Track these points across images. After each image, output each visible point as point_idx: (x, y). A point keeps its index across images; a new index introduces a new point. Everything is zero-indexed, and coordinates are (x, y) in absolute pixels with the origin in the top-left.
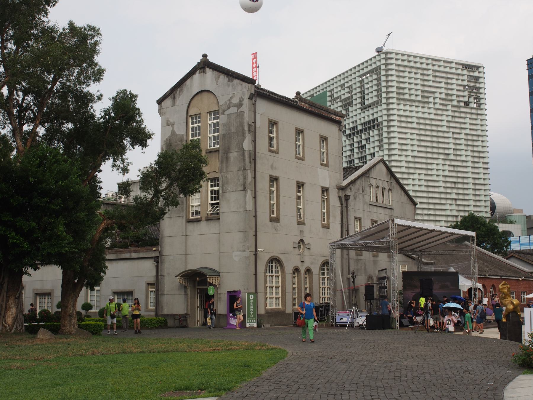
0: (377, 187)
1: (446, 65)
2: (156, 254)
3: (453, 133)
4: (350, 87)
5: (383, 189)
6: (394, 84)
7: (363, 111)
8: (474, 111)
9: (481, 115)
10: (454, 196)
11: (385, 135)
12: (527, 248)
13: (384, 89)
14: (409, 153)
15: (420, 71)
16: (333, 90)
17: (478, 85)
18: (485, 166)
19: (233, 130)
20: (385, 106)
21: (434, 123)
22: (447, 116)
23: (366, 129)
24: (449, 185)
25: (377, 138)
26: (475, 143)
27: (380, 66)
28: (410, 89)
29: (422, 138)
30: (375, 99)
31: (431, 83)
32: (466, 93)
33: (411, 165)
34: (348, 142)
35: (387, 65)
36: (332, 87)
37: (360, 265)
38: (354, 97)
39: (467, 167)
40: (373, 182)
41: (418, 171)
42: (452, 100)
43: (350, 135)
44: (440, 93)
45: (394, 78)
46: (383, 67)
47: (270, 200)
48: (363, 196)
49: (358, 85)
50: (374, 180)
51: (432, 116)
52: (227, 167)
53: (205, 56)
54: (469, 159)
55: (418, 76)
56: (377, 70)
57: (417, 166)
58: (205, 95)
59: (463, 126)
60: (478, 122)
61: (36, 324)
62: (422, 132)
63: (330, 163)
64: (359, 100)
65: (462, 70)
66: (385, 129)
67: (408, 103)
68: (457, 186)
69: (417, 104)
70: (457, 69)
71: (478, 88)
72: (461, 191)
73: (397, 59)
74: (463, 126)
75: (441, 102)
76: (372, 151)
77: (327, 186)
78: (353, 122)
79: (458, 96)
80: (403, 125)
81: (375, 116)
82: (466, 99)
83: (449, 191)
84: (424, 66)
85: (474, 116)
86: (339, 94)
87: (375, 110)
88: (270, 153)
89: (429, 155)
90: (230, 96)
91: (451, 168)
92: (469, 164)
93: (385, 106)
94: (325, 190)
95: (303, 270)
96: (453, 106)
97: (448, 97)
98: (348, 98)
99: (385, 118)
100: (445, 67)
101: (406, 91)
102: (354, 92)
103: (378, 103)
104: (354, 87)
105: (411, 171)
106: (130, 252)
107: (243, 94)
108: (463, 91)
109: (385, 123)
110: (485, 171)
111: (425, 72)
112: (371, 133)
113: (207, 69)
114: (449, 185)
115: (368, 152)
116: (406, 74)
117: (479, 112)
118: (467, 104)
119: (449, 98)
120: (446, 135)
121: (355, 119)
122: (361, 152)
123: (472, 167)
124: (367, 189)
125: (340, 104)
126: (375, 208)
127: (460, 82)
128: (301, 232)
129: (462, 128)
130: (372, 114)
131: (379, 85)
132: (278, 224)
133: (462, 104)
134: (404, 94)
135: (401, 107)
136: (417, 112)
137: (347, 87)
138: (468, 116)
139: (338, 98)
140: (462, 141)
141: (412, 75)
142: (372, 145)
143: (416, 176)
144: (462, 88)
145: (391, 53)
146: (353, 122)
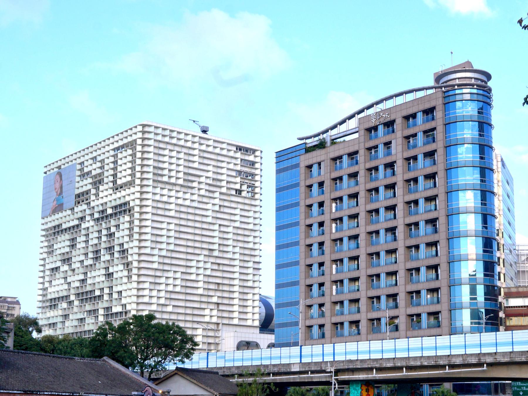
1: (216, 145)
3: (220, 225)
4: (102, 161)
6: (151, 162)
7: (115, 191)
8: (247, 201)
11: (137, 222)
13: (138, 168)
14: (164, 246)
16: (83, 162)
17: (253, 171)
18: (256, 266)
20: (138, 188)
22: (214, 205)
25: (127, 225)
27: (135, 140)
28: (170, 170)
29: (183, 229)
30: (129, 178)
31: (196, 165)
32: (238, 180)
33: (167, 261)
35: (143, 139)
38: (106, 174)
42: (221, 187)
43: (98, 219)
45: (151, 156)
46: (139, 142)
49: (112, 159)
51: (195, 204)
54: (237, 256)
56: (132, 145)
57: (174, 262)
61: (136, 393)
62: (183, 222)
64: (111, 178)
66: (137, 216)
68: (221, 288)
69: (178, 188)
70: (229, 150)
71: (253, 175)
75: (207, 188)
76: (121, 241)
79: (228, 182)
80: (160, 212)
82: (238, 187)
87: (128, 191)
89: (190, 250)
91: (215, 267)
93: (138, 188)
96: (221, 193)
97: (216, 183)
98: (100, 175)
99: (138, 202)
100: (215, 147)
101: (166, 172)
103: (131, 184)
104: (107, 161)
105: (166, 268)
108: (235, 177)
109: (137, 209)
110: (256, 272)
112: (122, 220)
117: (253, 202)
118: (239, 192)
120: (211, 227)
121: (105, 200)
122: (109, 241)
125: (90, 180)
127: (231, 166)
129: (231, 220)
133: (234, 192)
134: (162, 176)
136: (175, 198)
137: (99, 161)
138: (241, 206)
140: (230, 236)
141: (174, 154)
142: (121, 233)
143: (171, 274)
144: (234, 174)
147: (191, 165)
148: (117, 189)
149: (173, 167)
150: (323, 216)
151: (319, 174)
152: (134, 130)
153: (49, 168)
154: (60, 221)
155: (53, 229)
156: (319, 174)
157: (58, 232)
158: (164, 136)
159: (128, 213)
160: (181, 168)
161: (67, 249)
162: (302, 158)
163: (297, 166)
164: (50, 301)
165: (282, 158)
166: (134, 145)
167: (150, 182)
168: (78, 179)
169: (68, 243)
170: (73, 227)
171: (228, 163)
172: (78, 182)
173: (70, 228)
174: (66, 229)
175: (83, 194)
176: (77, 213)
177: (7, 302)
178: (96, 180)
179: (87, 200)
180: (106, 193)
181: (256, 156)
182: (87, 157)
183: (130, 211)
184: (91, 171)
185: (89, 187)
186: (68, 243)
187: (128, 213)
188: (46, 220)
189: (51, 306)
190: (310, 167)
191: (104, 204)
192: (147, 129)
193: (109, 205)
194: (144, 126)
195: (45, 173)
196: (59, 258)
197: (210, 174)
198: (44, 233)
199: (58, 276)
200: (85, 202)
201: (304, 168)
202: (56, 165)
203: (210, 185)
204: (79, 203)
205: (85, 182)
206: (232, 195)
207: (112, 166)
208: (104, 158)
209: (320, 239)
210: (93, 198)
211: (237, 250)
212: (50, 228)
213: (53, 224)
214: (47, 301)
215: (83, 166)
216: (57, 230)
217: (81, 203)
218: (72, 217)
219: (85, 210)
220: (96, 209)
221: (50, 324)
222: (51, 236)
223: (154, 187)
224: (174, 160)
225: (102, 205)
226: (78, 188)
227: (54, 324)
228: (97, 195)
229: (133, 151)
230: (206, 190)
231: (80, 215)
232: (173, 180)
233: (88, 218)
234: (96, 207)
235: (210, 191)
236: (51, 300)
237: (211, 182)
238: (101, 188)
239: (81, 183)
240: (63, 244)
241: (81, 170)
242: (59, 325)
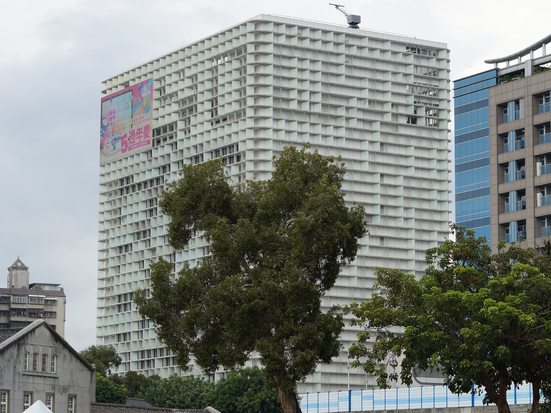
1: (374, 45)
3: (382, 175)
4: (194, 77)
6: (269, 81)
7: (215, 126)
8: (425, 134)
9: (440, 141)
13: (250, 91)
15: (321, 58)
20: (251, 123)
22: (372, 142)
26: (425, 196)
28: (300, 92)
30: (235, 107)
31: (342, 81)
35: (257, 44)
36: (162, 73)
38: (200, 98)
39: (407, 240)
42: (382, 113)
46: (251, 49)
50: (32, 347)
51: (343, 144)
54: (412, 224)
55: (318, 67)
56: (240, 52)
59: (403, 162)
60: (434, 154)
65: (405, 55)
67: (296, 118)
69: (313, 120)
73: (277, 35)
74: (403, 162)
75: (361, 115)
79: (393, 105)
81: (234, 139)
82: (410, 111)
84: (330, 48)
86: (174, 88)
91: (377, 243)
92: (412, 235)
93: (251, 123)
98: (190, 99)
99: (250, 145)
101: (294, 95)
102: (200, 88)
103: (239, 114)
104: (200, 78)
108: (406, 95)
109: (250, 156)
111: (333, 59)
116: (294, 63)
117: (436, 135)
118: (413, 120)
119: (378, 108)
120: (368, 179)
121: (199, 140)
123: (417, 241)
126: (31, 378)
127: (400, 79)
133: (404, 121)
134: (288, 101)
135: (282, 125)
138: (414, 143)
139: (171, 96)
141: (307, 65)
145: (266, 23)
147: (333, 80)
148: (218, 122)
149: (306, 86)
150: (523, 181)
151: (517, 117)
152: (242, 30)
153: (109, 85)
154: (130, 172)
155: (119, 183)
156: (517, 117)
157: (127, 188)
158: (289, 37)
159: (235, 162)
160: (319, 88)
161: (142, 217)
162: (493, 91)
163: (485, 103)
164: (117, 299)
165: (463, 91)
166: (243, 54)
167: (269, 113)
168: (156, 104)
169: (143, 207)
170: (151, 181)
171: (394, 73)
172: (157, 109)
173: (145, 183)
174: (139, 185)
175: (165, 128)
176: (156, 158)
177: (44, 293)
178: (185, 107)
179: (171, 137)
180: (200, 129)
181: (439, 60)
182: (168, 70)
183: (238, 158)
184: (176, 93)
185: (175, 117)
186: (143, 207)
187: (235, 162)
188: (107, 169)
189: (119, 306)
190: (503, 107)
191: (199, 147)
192: (262, 28)
193: (206, 148)
194: (257, 23)
195: (104, 92)
196: (131, 230)
197: (366, 94)
198: (105, 189)
199: (129, 259)
200: (169, 141)
201: (495, 108)
202: (121, 80)
203: (364, 111)
204: (159, 142)
205: (168, 110)
206: (402, 125)
207: (208, 85)
208: (196, 72)
209: (520, 215)
210: (181, 135)
211: (412, 214)
212: (116, 182)
213: (119, 176)
214: (114, 297)
215: (163, 84)
216: (125, 185)
217: (162, 143)
218: (148, 166)
219: (169, 155)
220: (186, 154)
221: (119, 335)
222: (116, 193)
223: (276, 120)
224: (307, 76)
225: (195, 147)
226: (157, 119)
227: (125, 334)
228: (187, 131)
229: (241, 73)
230: (359, 120)
231: (161, 162)
232: (306, 107)
233: (174, 168)
234: (185, 151)
235: (364, 121)
236: (119, 296)
237: (367, 106)
238: (193, 121)
239: (161, 112)
240: (135, 209)
241: (161, 90)
242: (134, 337)
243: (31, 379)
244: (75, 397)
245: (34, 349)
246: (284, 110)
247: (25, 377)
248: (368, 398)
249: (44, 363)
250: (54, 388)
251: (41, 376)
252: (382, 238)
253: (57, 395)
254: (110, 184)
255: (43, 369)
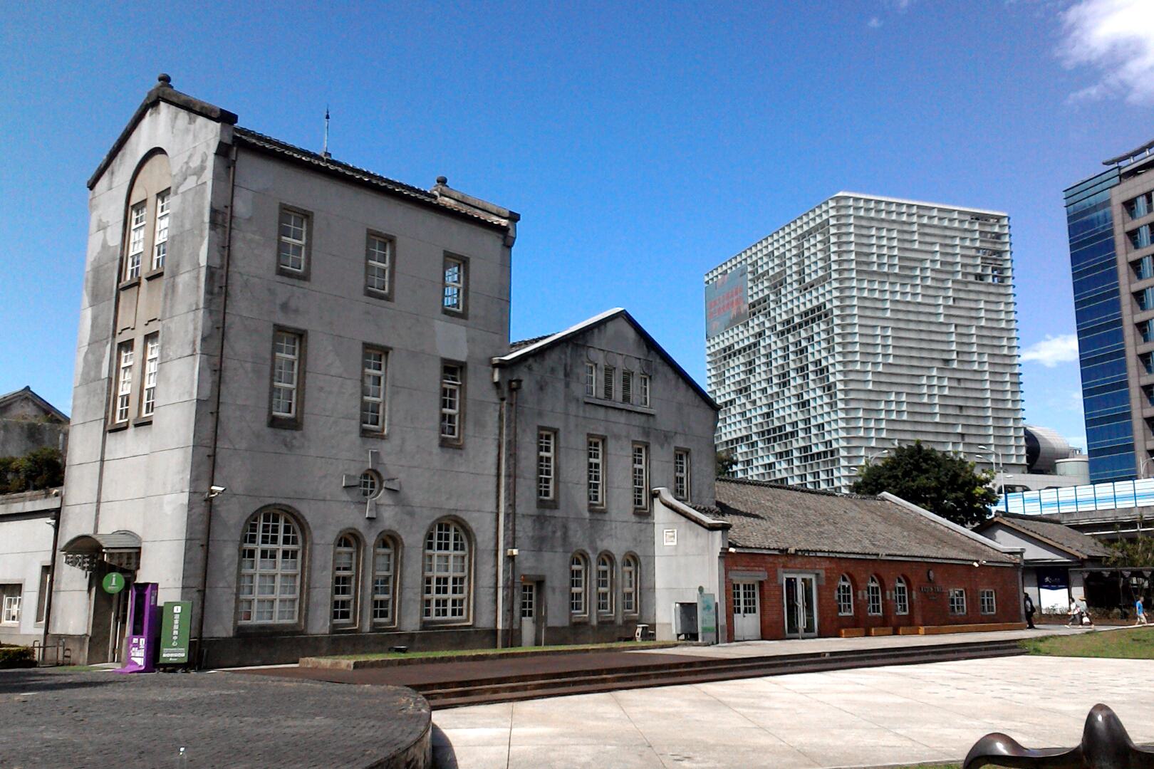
0: (609, 371)
1: (943, 215)
2: (53, 503)
5: (627, 377)
8: (992, 289)
10: (959, 430)
12: (1053, 510)
18: (1015, 380)
19: (187, 226)
21: (921, 309)
23: (807, 323)
24: (950, 411)
31: (916, 246)
34: (780, 344)
37: (550, 529)
38: (788, 272)
40: (600, 359)
41: (896, 389)
43: (782, 333)
44: (933, 261)
47: (272, 380)
48: (567, 385)
50: (601, 355)
51: (919, 299)
52: (172, 307)
53: (165, 79)
58: (158, 157)
62: (902, 325)
63: (471, 311)
69: (892, 279)
72: (972, 422)
77: (463, 359)
78: (786, 312)
82: (979, 270)
83: (951, 420)
85: (992, 298)
86: (765, 268)
88: (279, 278)
90: (188, 154)
91: (955, 384)
94: (452, 369)
95: (371, 539)
103: (825, 279)
106: (24, 499)
107: (208, 145)
112: (816, 329)
113: (162, 104)
114: (950, 411)
115: (811, 359)
117: (1002, 290)
118: (980, 277)
119: (949, 268)
120: (944, 329)
124: (581, 371)
127: (968, 243)
128: (376, 455)
130: (817, 298)
131: (826, 250)
132: (297, 434)
133: (972, 279)
136: (890, 292)
138: (983, 297)
139: (763, 275)
144: (973, 252)
146: (786, 312)
161: (743, 376)
175: (759, 302)
228: (778, 301)
231: (757, 330)
243: (601, 413)
244: (687, 452)
245: (605, 357)
246: (865, 272)
247: (587, 407)
248: (1033, 500)
249: (626, 387)
250: (647, 432)
251: (622, 410)
252: (959, 380)
253: (655, 448)
254: (714, 354)
255: (626, 399)
